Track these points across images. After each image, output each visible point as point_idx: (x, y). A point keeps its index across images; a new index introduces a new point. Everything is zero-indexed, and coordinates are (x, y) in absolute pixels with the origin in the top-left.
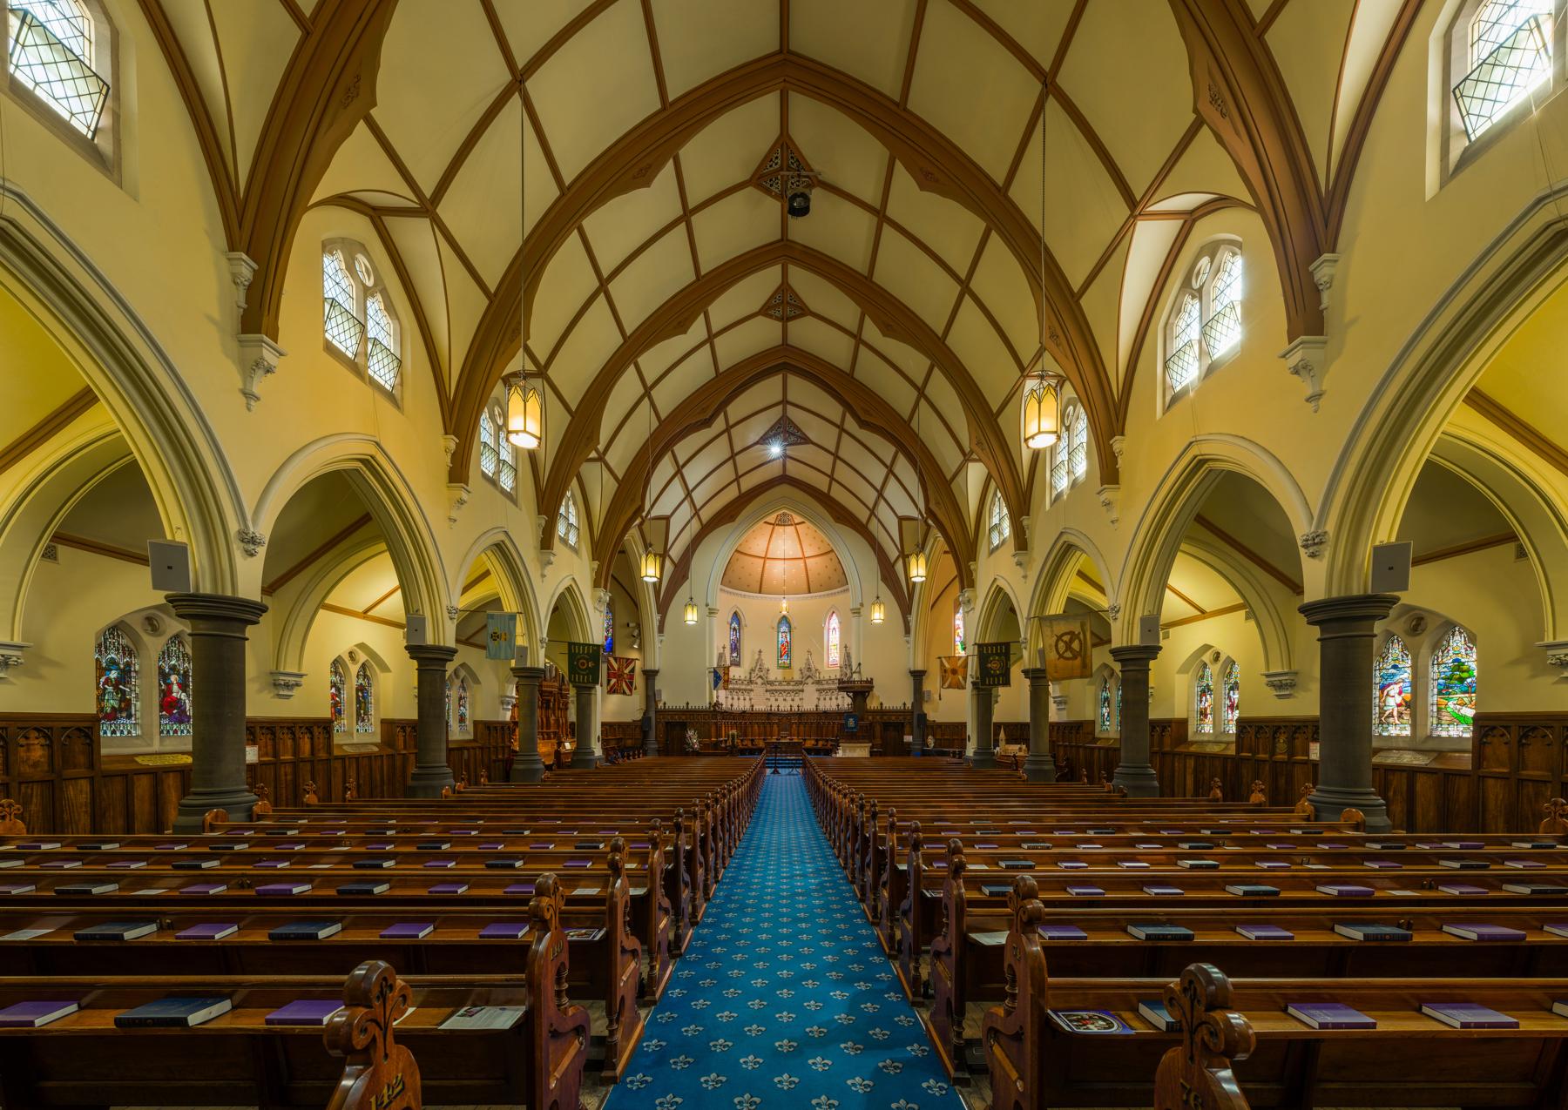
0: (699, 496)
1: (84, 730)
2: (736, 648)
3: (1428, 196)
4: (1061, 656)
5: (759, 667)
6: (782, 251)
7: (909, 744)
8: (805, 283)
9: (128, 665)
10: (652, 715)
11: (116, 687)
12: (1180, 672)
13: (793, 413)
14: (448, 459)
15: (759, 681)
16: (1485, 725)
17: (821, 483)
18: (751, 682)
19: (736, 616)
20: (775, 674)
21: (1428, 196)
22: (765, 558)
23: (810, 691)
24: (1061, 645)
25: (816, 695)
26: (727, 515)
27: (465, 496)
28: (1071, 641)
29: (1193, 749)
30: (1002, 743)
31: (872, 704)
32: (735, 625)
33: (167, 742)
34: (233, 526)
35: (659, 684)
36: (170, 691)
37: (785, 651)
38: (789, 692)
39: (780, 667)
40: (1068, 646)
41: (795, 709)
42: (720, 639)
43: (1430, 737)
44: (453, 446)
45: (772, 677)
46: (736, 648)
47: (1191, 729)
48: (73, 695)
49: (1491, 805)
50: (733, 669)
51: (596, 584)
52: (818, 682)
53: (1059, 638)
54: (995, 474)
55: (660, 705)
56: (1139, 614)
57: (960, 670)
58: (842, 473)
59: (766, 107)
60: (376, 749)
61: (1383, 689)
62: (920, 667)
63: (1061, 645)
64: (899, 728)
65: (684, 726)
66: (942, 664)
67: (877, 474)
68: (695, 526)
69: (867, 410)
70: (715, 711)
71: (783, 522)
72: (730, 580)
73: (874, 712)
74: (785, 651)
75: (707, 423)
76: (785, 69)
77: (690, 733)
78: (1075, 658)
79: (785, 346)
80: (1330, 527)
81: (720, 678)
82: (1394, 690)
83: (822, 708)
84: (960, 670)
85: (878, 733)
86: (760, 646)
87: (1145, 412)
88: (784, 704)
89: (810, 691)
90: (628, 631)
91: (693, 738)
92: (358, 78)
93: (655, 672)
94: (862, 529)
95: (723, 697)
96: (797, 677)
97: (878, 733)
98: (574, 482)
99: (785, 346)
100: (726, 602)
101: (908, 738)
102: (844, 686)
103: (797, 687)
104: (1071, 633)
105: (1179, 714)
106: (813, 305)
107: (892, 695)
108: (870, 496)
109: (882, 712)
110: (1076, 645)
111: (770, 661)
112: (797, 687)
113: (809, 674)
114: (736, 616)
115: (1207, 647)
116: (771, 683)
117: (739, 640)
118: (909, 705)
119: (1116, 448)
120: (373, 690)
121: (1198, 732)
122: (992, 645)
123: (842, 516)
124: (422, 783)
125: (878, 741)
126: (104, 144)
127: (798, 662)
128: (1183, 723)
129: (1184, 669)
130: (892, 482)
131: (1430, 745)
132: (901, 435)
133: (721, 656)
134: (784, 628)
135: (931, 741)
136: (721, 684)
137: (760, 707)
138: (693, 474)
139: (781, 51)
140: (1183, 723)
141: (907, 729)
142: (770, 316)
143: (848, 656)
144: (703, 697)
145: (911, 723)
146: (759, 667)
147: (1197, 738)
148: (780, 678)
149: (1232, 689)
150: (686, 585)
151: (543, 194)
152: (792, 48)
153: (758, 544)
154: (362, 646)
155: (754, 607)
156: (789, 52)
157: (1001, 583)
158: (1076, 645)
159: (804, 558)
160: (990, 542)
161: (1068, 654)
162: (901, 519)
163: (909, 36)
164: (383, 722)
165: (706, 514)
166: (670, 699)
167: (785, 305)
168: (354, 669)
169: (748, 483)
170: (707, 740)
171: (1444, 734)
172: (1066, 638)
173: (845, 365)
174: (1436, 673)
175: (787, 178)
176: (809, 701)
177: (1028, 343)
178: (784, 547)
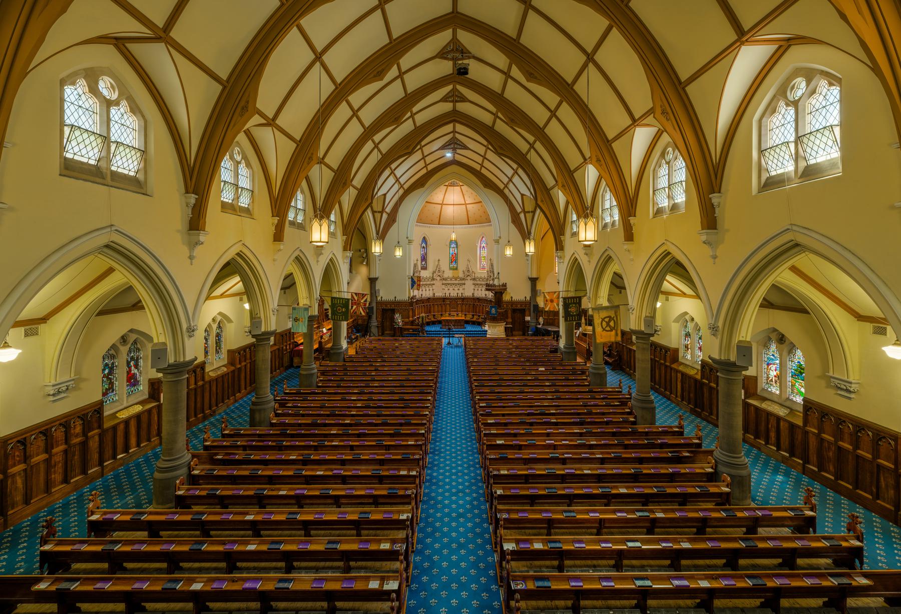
0: (402, 180)
1: (98, 408)
2: (424, 258)
3: (754, 194)
4: (604, 330)
5: (438, 269)
6: (454, 117)
7: (528, 322)
8: (466, 38)
9: (113, 364)
10: (374, 305)
11: (107, 378)
12: (674, 321)
13: (457, 136)
14: (274, 228)
15: (438, 278)
16: (809, 406)
17: (478, 167)
18: (433, 279)
19: (424, 240)
20: (448, 274)
21: (754, 194)
22: (442, 204)
23: (469, 283)
24: (604, 323)
25: (473, 287)
26: (420, 183)
27: (282, 247)
28: (610, 321)
29: (681, 368)
30: (583, 325)
31: (506, 298)
32: (424, 245)
33: (130, 399)
34: (185, 326)
35: (378, 285)
36: (130, 370)
37: (454, 259)
38: (456, 284)
39: (451, 269)
40: (608, 324)
41: (460, 295)
42: (416, 254)
43: (788, 399)
44: (276, 222)
45: (446, 276)
46: (424, 258)
47: (681, 355)
48: (90, 394)
49: (811, 447)
50: (422, 272)
51: (345, 249)
52: (474, 279)
53: (603, 320)
54: (571, 200)
55: (379, 298)
56: (644, 315)
57: (555, 300)
58: (486, 163)
59: (449, 128)
60: (225, 369)
61: (768, 365)
62: (534, 276)
63: (604, 323)
64: (523, 312)
65: (393, 311)
66: (545, 297)
67: (510, 172)
68: (401, 192)
69: (504, 148)
70: (412, 303)
71: (453, 185)
72: (421, 220)
73: (508, 302)
74: (454, 259)
75: (410, 154)
76: (454, 19)
77: (397, 316)
78: (611, 330)
79: (455, 111)
80: (720, 324)
81: (415, 282)
82: (773, 367)
83: (476, 295)
84: (555, 300)
85: (510, 315)
86: (439, 257)
87: (644, 211)
88: (453, 292)
89: (469, 283)
90: (359, 253)
91: (399, 319)
92: (248, 102)
93: (376, 279)
94: (500, 192)
95: (416, 293)
96: (461, 275)
97: (510, 315)
98: (337, 206)
99: (455, 111)
100: (417, 232)
101: (528, 318)
102: (489, 287)
103: (461, 281)
104: (610, 317)
105: (673, 344)
106: (473, 50)
107: (518, 292)
108: (506, 180)
109: (512, 303)
110: (612, 324)
111: (445, 265)
112: (461, 281)
113: (468, 273)
114: (424, 240)
115: (686, 313)
116: (445, 279)
117: (426, 254)
118: (528, 298)
119: (632, 222)
120: (223, 334)
121: (684, 357)
122: (571, 298)
123: (488, 184)
124: (258, 407)
125: (510, 320)
126: (141, 176)
127: (462, 266)
128: (676, 351)
129: (677, 320)
130: (516, 176)
131: (788, 404)
132: (522, 161)
133: (415, 265)
134: (453, 245)
135: (541, 320)
136: (415, 286)
137: (439, 294)
138: (398, 173)
139: (453, 12)
140: (676, 351)
141: (527, 313)
142: (446, 58)
143: (492, 265)
144: (405, 293)
145: (530, 310)
146: (438, 269)
147: (683, 361)
148: (451, 276)
149: (700, 338)
150: (395, 225)
151: (328, 88)
152: (459, 10)
153: (438, 196)
154: (220, 314)
155: (434, 233)
156: (457, 13)
157: (576, 255)
158: (612, 324)
159: (466, 204)
160: (572, 229)
161: (608, 328)
162: (522, 195)
163: (520, 17)
164: (229, 351)
165: (406, 186)
166: (385, 294)
167: (454, 51)
168: (215, 326)
169: (430, 167)
170: (407, 320)
171: (794, 399)
172: (607, 320)
173: (490, 124)
174: (791, 366)
175: (454, 51)
176: (469, 290)
177: (588, 155)
178: (454, 198)
